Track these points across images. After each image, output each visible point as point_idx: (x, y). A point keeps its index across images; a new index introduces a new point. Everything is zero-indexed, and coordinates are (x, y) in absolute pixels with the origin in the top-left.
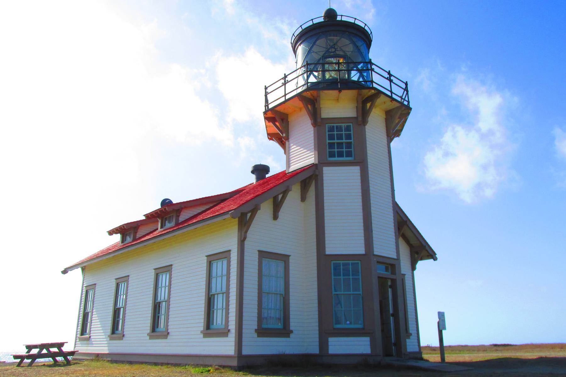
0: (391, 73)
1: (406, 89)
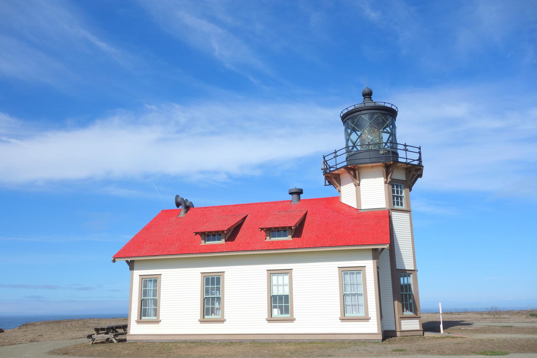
1: (420, 153)
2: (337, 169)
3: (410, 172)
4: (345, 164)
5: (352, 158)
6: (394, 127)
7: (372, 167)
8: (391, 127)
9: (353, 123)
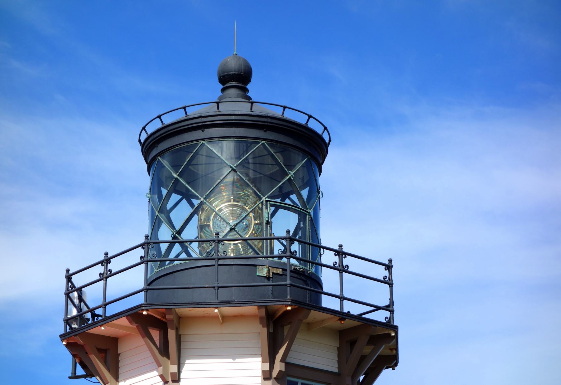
0: (345, 250)
1: (388, 281)
2: (107, 320)
3: (353, 344)
4: (140, 299)
5: (166, 283)
6: (315, 192)
7: (225, 319)
8: (305, 193)
9: (175, 167)
